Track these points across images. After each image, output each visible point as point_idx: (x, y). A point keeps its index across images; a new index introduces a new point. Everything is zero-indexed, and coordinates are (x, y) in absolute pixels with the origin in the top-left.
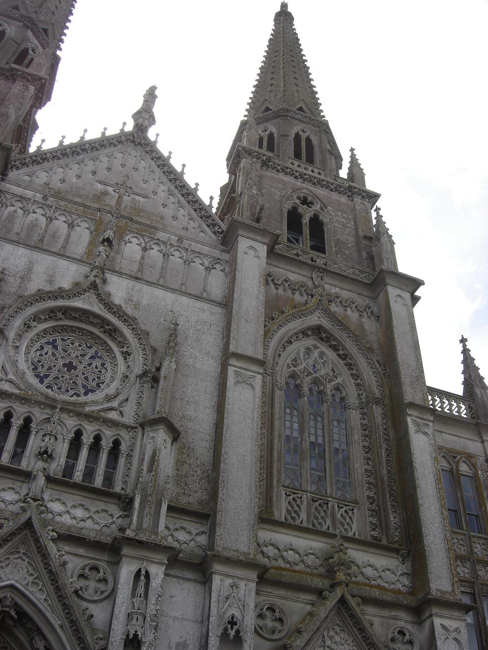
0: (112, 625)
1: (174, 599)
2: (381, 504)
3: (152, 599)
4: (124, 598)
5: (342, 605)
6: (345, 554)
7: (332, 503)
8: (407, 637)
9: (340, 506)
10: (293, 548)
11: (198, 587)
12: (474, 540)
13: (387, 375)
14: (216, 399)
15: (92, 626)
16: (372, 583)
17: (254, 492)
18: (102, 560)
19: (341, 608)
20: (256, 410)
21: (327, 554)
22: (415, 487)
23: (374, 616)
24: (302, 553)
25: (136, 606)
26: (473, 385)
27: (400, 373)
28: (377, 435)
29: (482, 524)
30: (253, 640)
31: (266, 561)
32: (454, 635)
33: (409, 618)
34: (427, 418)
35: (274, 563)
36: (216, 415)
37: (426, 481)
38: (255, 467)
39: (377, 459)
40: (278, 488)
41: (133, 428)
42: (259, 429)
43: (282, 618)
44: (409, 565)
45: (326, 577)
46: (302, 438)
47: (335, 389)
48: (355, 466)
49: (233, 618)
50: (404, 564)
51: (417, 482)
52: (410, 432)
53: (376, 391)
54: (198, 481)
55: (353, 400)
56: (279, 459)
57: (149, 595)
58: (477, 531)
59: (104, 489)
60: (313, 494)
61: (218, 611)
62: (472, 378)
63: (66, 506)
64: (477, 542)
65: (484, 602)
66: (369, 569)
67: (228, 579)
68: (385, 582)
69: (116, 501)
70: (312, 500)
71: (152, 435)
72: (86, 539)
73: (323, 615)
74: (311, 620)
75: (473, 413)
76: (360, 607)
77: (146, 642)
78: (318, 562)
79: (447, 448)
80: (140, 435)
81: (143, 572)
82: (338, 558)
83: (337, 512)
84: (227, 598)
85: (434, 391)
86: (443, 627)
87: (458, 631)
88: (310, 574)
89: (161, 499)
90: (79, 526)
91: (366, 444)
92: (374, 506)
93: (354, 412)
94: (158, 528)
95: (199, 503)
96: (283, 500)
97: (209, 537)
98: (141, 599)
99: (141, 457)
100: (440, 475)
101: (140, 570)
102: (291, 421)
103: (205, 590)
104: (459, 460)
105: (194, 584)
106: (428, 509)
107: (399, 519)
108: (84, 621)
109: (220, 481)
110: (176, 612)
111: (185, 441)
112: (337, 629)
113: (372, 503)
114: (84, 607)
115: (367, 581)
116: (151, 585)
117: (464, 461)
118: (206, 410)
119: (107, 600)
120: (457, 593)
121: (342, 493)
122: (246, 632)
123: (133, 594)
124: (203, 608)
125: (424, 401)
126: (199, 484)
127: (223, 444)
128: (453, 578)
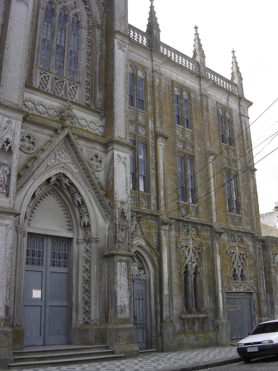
5: (67, 138)
6: (71, 111)
7: (66, 81)
8: (99, 159)
12: (139, 113)
13: (106, 12)
16: (83, 128)
19: (66, 140)
20: (28, 20)
21: (61, 110)
22: (113, 80)
23: (83, 146)
26: (152, 28)
27: (115, 12)
29: (144, 105)
30: (18, 153)
31: (27, 110)
32: (123, 160)
33: (101, 149)
36: (3, 19)
37: (120, 77)
38: (25, 55)
44: (104, 122)
45: (60, 122)
47: (75, 15)
49: (8, 140)
50: (101, 120)
52: (115, 48)
53: (99, 21)
55: (84, 23)
56: (38, 52)
66: (83, 120)
67: (6, 118)
70: (55, 79)
73: (57, 143)
74: (50, 145)
76: (77, 140)
78: (56, 114)
79: (133, 61)
82: (68, 113)
83: (68, 87)
84: (5, 128)
85: (135, 29)
86: (119, 156)
88: (51, 120)
92: (89, 87)
93: (84, 31)
96: (38, 77)
100: (127, 75)
102: (47, 30)
106: (119, 93)
107: (102, 96)
112: (63, 150)
113: (88, 85)
115: (81, 127)
117: (140, 70)
122: (15, 148)
127: (7, 38)
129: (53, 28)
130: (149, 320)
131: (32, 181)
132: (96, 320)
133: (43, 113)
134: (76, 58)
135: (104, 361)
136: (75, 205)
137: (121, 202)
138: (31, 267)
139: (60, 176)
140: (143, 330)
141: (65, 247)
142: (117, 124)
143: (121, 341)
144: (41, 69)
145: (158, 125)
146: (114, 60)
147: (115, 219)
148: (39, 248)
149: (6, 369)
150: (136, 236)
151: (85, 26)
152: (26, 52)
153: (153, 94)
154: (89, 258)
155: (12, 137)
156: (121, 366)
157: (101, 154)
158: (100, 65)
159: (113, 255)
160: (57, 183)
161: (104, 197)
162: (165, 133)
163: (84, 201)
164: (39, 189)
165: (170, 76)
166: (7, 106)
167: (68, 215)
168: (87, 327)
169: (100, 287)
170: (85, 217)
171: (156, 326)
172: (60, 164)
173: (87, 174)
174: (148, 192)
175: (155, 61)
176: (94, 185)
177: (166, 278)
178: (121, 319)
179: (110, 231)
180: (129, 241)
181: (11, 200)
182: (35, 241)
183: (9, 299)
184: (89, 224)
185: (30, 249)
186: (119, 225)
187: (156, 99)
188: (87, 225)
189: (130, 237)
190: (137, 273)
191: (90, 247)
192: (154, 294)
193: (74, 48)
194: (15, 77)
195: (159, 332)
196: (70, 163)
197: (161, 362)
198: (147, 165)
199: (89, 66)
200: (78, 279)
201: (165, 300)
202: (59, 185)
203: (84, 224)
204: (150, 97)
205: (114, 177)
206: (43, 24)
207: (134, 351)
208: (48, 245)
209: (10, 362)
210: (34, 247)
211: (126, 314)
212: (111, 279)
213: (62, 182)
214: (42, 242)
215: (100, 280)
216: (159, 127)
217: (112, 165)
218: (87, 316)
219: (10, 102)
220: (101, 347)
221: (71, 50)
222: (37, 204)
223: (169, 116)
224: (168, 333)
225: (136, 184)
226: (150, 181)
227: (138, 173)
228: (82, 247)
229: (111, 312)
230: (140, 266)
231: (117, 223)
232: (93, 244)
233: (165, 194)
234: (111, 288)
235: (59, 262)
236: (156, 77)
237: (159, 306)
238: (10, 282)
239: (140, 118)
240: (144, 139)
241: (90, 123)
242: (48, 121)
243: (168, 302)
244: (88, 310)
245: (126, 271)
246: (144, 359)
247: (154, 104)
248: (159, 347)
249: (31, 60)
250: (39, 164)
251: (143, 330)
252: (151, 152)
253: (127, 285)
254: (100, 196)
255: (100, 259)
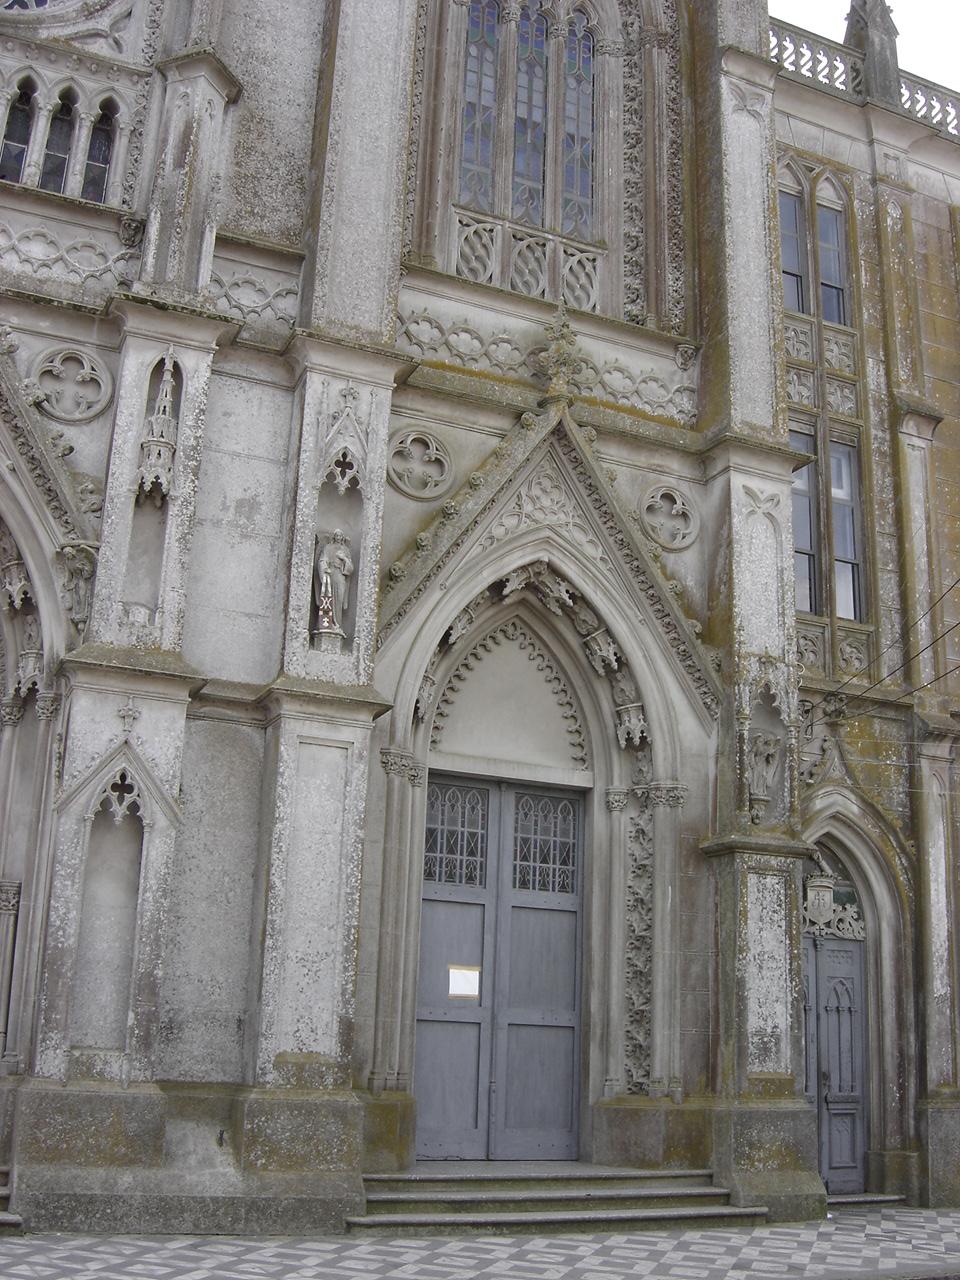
0: (111, 467)
1: (233, 419)
2: (651, 251)
3: (188, 416)
4: (131, 415)
7: (554, 243)
8: (678, 506)
9: (570, 251)
10: (470, 327)
11: (280, 398)
14: (319, 17)
15: (73, 468)
16: (620, 402)
17: (394, 213)
18: (87, 342)
19: (556, 445)
20: (404, 42)
21: (536, 343)
22: (721, 223)
23: (619, 463)
24: (487, 339)
25: (157, 429)
26: (866, 23)
28: (656, 112)
29: (847, 306)
30: (383, 497)
31: (414, 351)
33: (687, 472)
34: (762, 83)
35: (429, 356)
39: (650, 160)
40: (446, 208)
41: (141, 75)
42: (409, 84)
43: (442, 459)
45: (533, 387)
46: (500, 109)
47: (575, 10)
48: (606, 172)
49: (345, 455)
51: (728, 212)
52: (723, 109)
54: (280, 188)
55: (611, 36)
57: (181, 409)
58: (836, 319)
59: (84, 201)
60: (517, 224)
61: (317, 442)
62: (868, 7)
63: (10, 237)
64: (834, 340)
65: (832, 454)
68: (646, 402)
69: (113, 227)
71: (182, 89)
72: (53, 301)
75: (860, 83)
77: (177, 498)
78: (518, 357)
79: (796, 150)
80: (158, 92)
81: (169, 366)
82: (558, 350)
86: (748, 492)
87: (775, 500)
88: (500, 380)
89: (203, 223)
90: (39, 277)
91: (630, 128)
92: (636, 256)
93: (613, 60)
94: (197, 281)
95: (283, 233)
97: (302, 301)
98: (167, 416)
99: (161, 136)
101: (162, 362)
103: (293, 402)
104: (819, 175)
105: (271, 391)
107: (684, 282)
108: (56, 458)
109: (325, 189)
110: (237, 444)
111: (252, 104)
112: (547, 483)
113: (633, 249)
114: (55, 434)
116: (184, 390)
117: (827, 179)
118: (298, 41)
119: (101, 419)
120: (782, 431)
121: (576, 225)
122: (371, 480)
123: (150, 408)
124: (289, 436)
125: (760, 45)
126: (283, 194)
127: (332, 112)
128: (777, 403)
129: (501, 63)
130: (874, 1085)
131: (438, 594)
132: (670, 1078)
133: (473, 359)
134: (587, 158)
135: (692, 1228)
136: (597, 671)
137: (760, 659)
138: (442, 890)
139: (539, 574)
140: (854, 1122)
141: (565, 821)
142: (742, 379)
143: (759, 1161)
144: (463, 208)
145: (902, 374)
146: (719, 151)
147: (738, 719)
148: (473, 824)
149: (337, 1232)
150: (826, 780)
151: (615, 43)
152: (400, 154)
153: (880, 263)
154: (647, 858)
155: (359, 446)
156: (878, 1254)
157: (685, 490)
158: (674, 176)
159: (730, 851)
160: (531, 597)
161: (699, 641)
162: (929, 401)
163: (627, 659)
164: (464, 620)
165: (944, 194)
166: (338, 342)
167: (574, 709)
168: (638, 1102)
169: (688, 962)
170: (633, 713)
171: (902, 1110)
172: (537, 529)
173: (635, 563)
174: (868, 622)
175: (879, 141)
176: (660, 599)
177: (938, 935)
178: (761, 1080)
179: (722, 761)
180: (792, 797)
181: (362, 660)
182: (457, 801)
183: (354, 994)
184: (646, 738)
185: (439, 827)
186: (754, 741)
187: (893, 282)
188: (638, 743)
189: (795, 783)
190: (830, 916)
191: (650, 820)
192: (893, 992)
193: (578, 126)
194: (367, 241)
195: (912, 1132)
196: (571, 526)
197: (899, 1245)
198: (863, 522)
199: (636, 184)
200: (610, 936)
201: (937, 1017)
202: (538, 604)
203: (629, 740)
204: (866, 275)
205: (731, 570)
206: (462, 53)
207: (806, 1199)
208: (503, 811)
209: (354, 1211)
210: (453, 821)
211: (783, 1063)
212: (724, 933)
213: (545, 595)
214: (483, 805)
215: (686, 938)
216: (905, 381)
217: (725, 528)
218: (641, 1065)
219: (351, 329)
220: (685, 1177)
221: (569, 134)
222: (463, 672)
223: (943, 340)
224: (947, 1137)
225: (821, 592)
226: (876, 580)
227: (830, 554)
228: (625, 820)
229: (726, 1052)
230: (843, 890)
231: (746, 733)
232: (662, 811)
233: (933, 625)
234: (724, 966)
235: (544, 874)
236: (888, 201)
237: (912, 1038)
238: (357, 940)
239: (834, 354)
240: (848, 429)
241: (644, 381)
242: (489, 383)
243: (946, 1024)
244: (644, 1044)
245: (780, 905)
246: (840, 1229)
247: (883, 300)
248: (911, 1185)
249: (423, 181)
250: (460, 532)
251: (854, 1122)
252: (879, 473)
253: (785, 960)
254: (682, 638)
255: (687, 865)
